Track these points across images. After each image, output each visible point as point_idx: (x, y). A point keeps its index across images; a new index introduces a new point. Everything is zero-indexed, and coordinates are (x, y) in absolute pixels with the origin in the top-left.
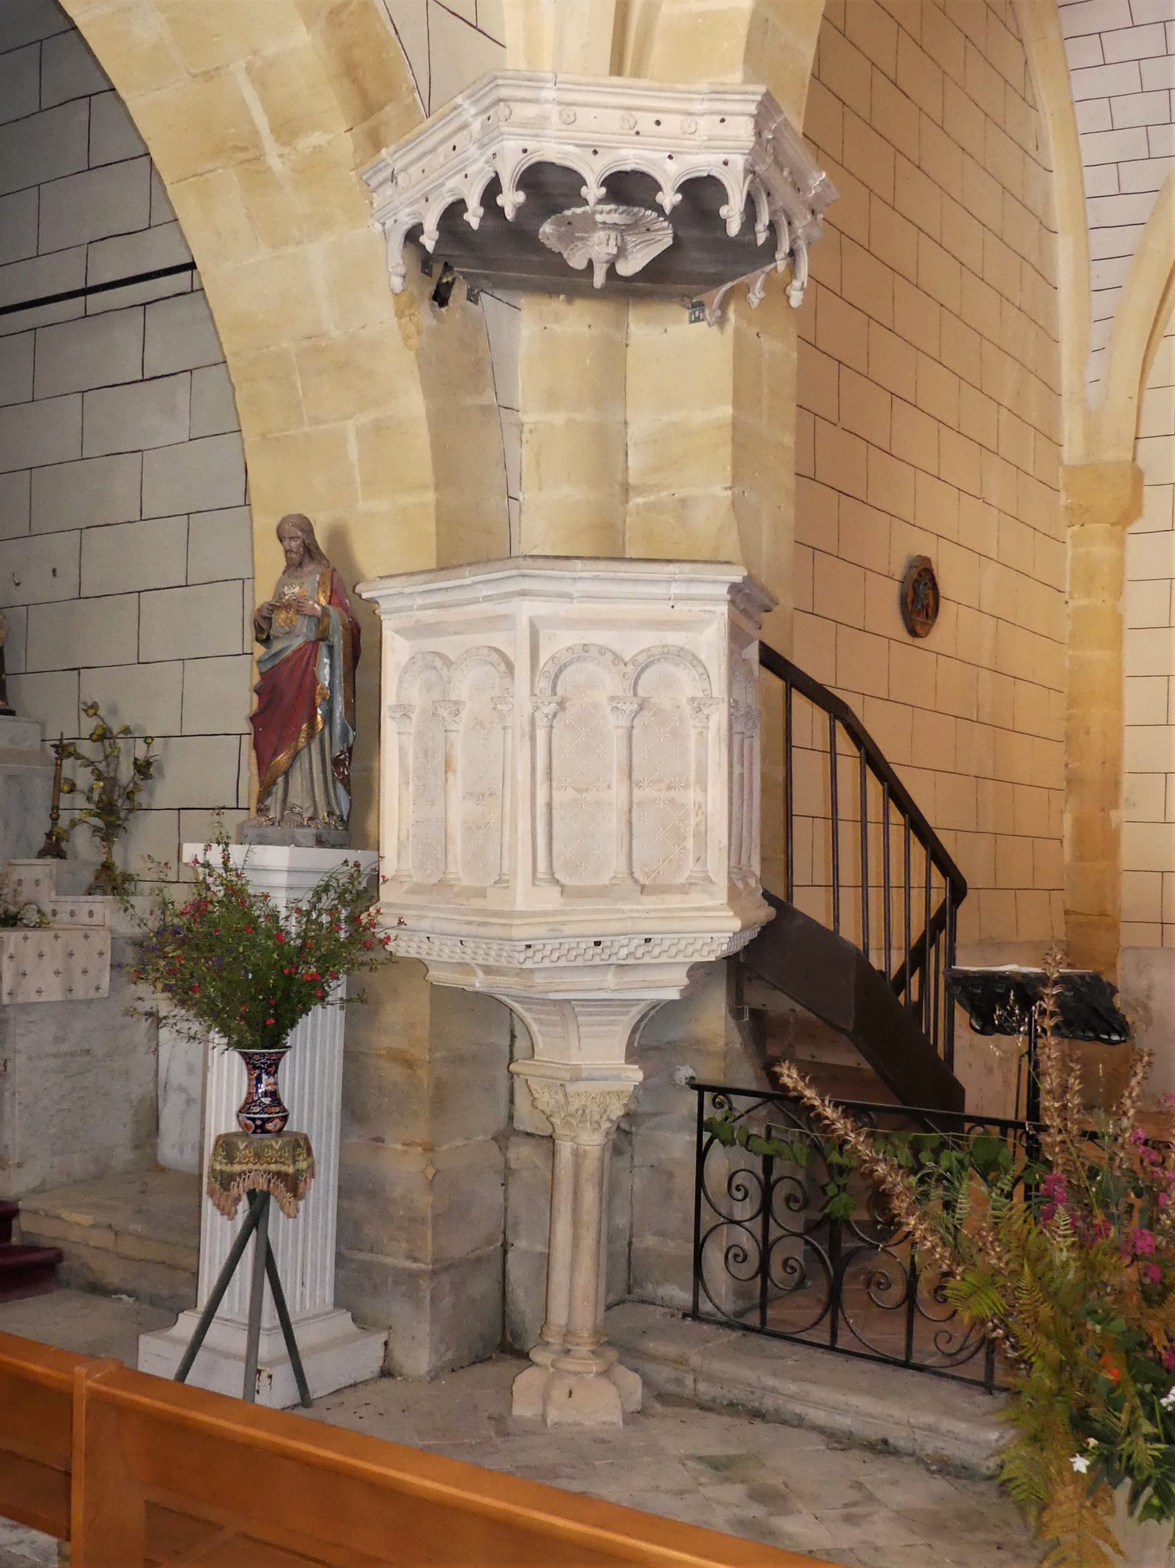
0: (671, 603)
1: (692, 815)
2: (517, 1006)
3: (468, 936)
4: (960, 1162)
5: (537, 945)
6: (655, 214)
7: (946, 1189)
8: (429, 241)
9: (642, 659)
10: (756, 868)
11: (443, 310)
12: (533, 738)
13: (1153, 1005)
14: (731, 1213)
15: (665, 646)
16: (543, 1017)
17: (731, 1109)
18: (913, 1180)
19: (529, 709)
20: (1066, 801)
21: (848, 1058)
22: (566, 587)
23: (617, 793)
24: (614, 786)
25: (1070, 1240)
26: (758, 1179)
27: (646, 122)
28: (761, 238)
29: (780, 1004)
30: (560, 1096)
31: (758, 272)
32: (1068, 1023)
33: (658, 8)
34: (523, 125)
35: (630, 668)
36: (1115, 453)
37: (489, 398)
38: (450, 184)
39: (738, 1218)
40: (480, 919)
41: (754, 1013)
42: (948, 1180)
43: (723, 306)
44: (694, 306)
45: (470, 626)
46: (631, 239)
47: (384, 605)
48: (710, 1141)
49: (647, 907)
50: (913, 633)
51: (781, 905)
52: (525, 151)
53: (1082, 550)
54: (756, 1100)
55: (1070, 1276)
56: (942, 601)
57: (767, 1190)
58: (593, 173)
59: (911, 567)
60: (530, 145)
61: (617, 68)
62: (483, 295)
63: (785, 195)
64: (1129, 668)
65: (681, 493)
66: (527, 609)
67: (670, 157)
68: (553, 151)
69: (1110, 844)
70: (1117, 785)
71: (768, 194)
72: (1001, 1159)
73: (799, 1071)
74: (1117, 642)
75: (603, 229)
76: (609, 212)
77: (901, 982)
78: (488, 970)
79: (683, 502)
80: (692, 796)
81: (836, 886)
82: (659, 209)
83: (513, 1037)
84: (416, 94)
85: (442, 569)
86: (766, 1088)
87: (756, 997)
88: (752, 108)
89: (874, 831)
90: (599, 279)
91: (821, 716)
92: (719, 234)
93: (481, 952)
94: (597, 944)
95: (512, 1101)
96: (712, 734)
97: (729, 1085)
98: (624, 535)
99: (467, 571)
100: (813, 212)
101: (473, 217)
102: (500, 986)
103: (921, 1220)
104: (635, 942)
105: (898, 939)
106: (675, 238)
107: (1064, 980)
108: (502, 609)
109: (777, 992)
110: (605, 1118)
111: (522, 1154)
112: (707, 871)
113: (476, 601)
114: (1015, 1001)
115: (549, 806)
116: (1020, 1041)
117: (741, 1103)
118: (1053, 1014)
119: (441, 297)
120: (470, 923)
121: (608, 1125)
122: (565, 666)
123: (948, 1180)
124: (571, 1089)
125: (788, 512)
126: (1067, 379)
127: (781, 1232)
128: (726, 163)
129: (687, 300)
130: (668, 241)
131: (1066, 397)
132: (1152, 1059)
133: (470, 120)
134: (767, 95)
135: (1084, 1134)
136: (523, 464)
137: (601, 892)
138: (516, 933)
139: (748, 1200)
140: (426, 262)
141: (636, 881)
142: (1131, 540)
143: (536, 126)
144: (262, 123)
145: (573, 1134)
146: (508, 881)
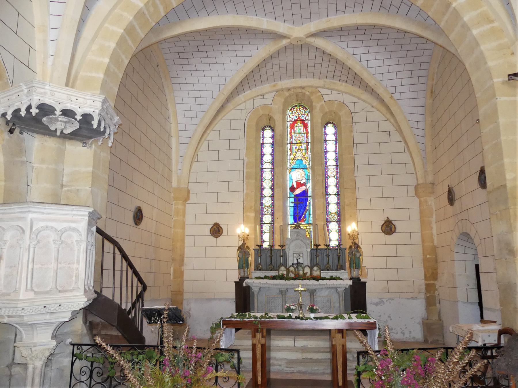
0: (73, 216)
1: (75, 271)
2: (18, 326)
3: (3, 307)
4: (143, 357)
5: (26, 308)
6: (75, 120)
7: (140, 365)
8: (9, 117)
9: (63, 230)
10: (92, 285)
11: (12, 135)
12: (29, 251)
13: (191, 312)
14: (80, 379)
15: (70, 227)
16: (26, 329)
17: (82, 350)
18: (130, 364)
19: (28, 243)
20: (172, 265)
21: (115, 332)
22: (45, 211)
23: (53, 265)
24: (53, 263)
25: (169, 375)
26: (89, 369)
27: (74, 99)
28: (102, 130)
29: (97, 319)
30: (30, 352)
31: (101, 137)
32: (170, 320)
33: (79, 73)
34: (39, 93)
35: (59, 233)
36: (184, 186)
37: (24, 159)
38: (17, 104)
39: (82, 380)
40: (8, 302)
41: (90, 323)
42: (140, 363)
43: (91, 144)
44: (84, 143)
46: (68, 125)
48: (76, 359)
49: (60, 296)
50: (136, 224)
51: (99, 294)
52: (39, 100)
53: (176, 207)
54: (89, 347)
55: (169, 384)
56: (143, 217)
57: (91, 371)
58: (58, 109)
59: (136, 209)
61: (67, 85)
62: (24, 133)
63: (108, 121)
64: (186, 234)
66: (30, 216)
67: (80, 108)
68: (48, 101)
69: (182, 274)
70: (183, 260)
71: (104, 120)
72: (153, 356)
73: (101, 338)
74: (183, 228)
75: (60, 122)
76: (62, 118)
77: (130, 312)
78: (9, 317)
79: (78, 190)
80: (75, 266)
81: (114, 288)
82: (76, 119)
83: (16, 335)
84: (9, 80)
85: (4, 204)
86: (93, 343)
87: (91, 318)
88: (101, 100)
89: (124, 273)
90: (58, 133)
91: (112, 246)
92: (91, 127)
93: (11, 311)
94: (45, 307)
95: (14, 354)
96: (81, 250)
97: (82, 343)
98: (61, 197)
99: (12, 205)
100: (115, 126)
101: (23, 113)
102: (12, 321)
103: (132, 375)
104: (56, 306)
105: (129, 300)
106: (80, 127)
107: (169, 309)
108: (22, 215)
109: (97, 317)
110: (44, 356)
111: (16, 370)
112: (78, 286)
113: (15, 213)
114: (157, 316)
115: (33, 269)
116: (158, 326)
117: (85, 348)
118: (166, 318)
119: (11, 131)
120: (4, 303)
121: (44, 358)
122: (41, 231)
123: (140, 363)
124: (33, 349)
125: (105, 194)
127: (95, 383)
128: (94, 111)
129: (82, 142)
130: (78, 127)
132: (190, 327)
133: (24, 89)
134: (105, 98)
135: (173, 347)
136: (33, 177)
137: (47, 293)
138: (19, 305)
139: (86, 375)
140: (7, 122)
141: (57, 289)
142: (187, 205)
145: (33, 363)
146: (17, 291)
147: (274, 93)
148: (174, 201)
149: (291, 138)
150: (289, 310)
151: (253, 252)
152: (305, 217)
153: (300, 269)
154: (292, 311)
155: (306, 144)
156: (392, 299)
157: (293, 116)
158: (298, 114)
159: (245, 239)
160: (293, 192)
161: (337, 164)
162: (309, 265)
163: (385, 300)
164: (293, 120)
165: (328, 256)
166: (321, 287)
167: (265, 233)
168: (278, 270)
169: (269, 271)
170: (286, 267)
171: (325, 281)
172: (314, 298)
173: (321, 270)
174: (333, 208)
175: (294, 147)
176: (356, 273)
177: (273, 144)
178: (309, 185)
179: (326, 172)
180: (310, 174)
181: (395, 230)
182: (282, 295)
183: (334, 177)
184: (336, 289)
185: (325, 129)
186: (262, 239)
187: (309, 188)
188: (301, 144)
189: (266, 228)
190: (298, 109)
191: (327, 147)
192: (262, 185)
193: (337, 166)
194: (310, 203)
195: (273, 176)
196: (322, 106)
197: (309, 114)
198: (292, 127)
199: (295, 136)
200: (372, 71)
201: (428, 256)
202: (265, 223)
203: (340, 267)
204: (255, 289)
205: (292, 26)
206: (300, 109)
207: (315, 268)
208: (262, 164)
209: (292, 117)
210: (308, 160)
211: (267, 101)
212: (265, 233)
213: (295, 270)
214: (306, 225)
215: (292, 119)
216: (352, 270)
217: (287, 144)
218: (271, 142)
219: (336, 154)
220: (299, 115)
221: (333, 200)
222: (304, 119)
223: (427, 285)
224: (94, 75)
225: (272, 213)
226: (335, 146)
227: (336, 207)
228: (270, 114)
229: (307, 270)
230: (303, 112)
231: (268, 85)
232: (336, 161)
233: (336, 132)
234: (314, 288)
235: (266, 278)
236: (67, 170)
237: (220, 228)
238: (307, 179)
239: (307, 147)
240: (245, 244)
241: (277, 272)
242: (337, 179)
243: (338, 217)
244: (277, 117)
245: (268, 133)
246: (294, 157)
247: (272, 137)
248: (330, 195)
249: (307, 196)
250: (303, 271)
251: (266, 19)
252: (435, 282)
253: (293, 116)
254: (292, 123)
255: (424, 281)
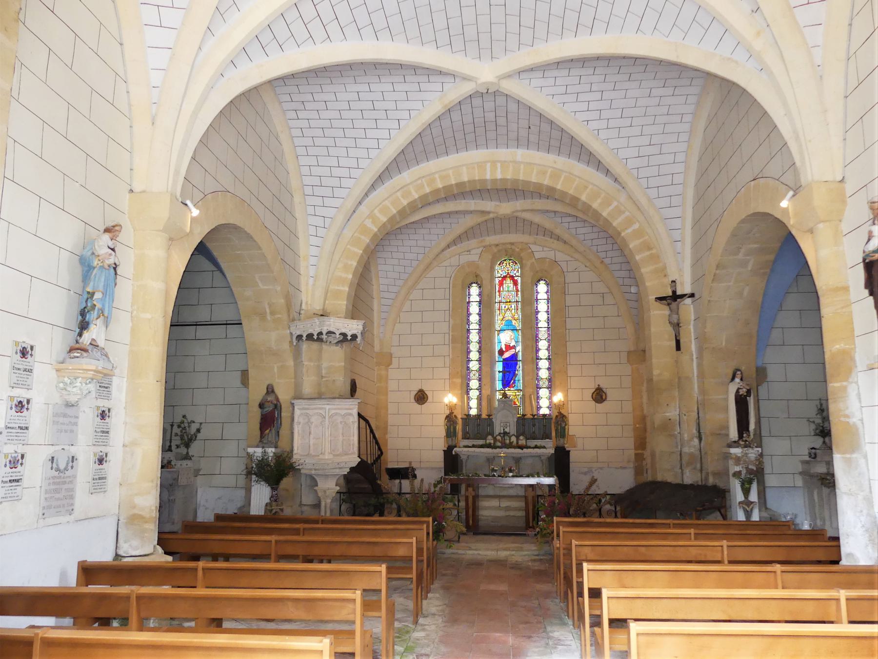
22: (334, 403)
45: (315, 409)
47: (295, 404)
48: (342, 503)
60: (328, 328)
65: (334, 378)
74: (387, 394)
78: (315, 470)
79: (334, 380)
80: (352, 438)
95: (301, 498)
108: (323, 406)
126: (375, 333)
131: (375, 336)
143: (330, 325)
144: (268, 311)
147: (481, 249)
148: (376, 366)
149: (500, 297)
150: (493, 470)
151: (460, 420)
152: (514, 383)
153: (507, 438)
154: (496, 471)
155: (516, 303)
156: (601, 468)
157: (502, 271)
158: (507, 269)
159: (452, 408)
160: (502, 356)
161: (548, 325)
162: (515, 434)
163: (593, 470)
164: (502, 276)
165: (534, 425)
166: (526, 455)
167: (472, 399)
168: (485, 439)
169: (477, 440)
170: (493, 436)
171: (541, 449)
172: (519, 466)
173: (527, 439)
174: (544, 374)
175: (503, 306)
176: (561, 442)
177: (480, 302)
178: (519, 348)
179: (537, 334)
180: (520, 337)
181: (606, 398)
182: (489, 463)
183: (545, 340)
184: (539, 456)
185: (536, 287)
186: (469, 405)
187: (519, 351)
188: (510, 303)
189: (474, 394)
190: (508, 264)
191: (538, 306)
192: (468, 348)
193: (548, 328)
194: (519, 367)
195: (480, 338)
196: (532, 264)
197: (519, 269)
198: (501, 284)
199: (504, 294)
200: (582, 237)
201: (637, 426)
202: (472, 389)
203: (547, 436)
204: (463, 457)
205: (498, 203)
206: (509, 263)
207: (521, 438)
208: (468, 325)
209: (501, 273)
210: (518, 321)
211: (474, 257)
212: (472, 399)
213: (502, 439)
214: (515, 391)
215: (501, 275)
216: (558, 439)
217: (496, 303)
218: (478, 300)
219: (548, 314)
220: (508, 270)
221: (544, 364)
222: (514, 275)
223: (636, 455)
224: (342, 288)
225: (479, 378)
226: (547, 306)
227: (547, 372)
228: (477, 272)
229: (514, 439)
230: (513, 267)
231: (475, 240)
232: (548, 323)
233: (548, 290)
234: (519, 456)
235: (474, 446)
236: (325, 364)
237: (424, 394)
238: (516, 342)
239: (517, 307)
240: (453, 413)
241: (484, 441)
242: (548, 342)
243: (548, 383)
244: (485, 276)
245: (474, 290)
246: (503, 318)
247: (480, 295)
248: (541, 359)
249: (517, 360)
250: (510, 440)
251: (473, 201)
252: (644, 452)
253: (502, 271)
254: (500, 279)
255: (633, 450)
